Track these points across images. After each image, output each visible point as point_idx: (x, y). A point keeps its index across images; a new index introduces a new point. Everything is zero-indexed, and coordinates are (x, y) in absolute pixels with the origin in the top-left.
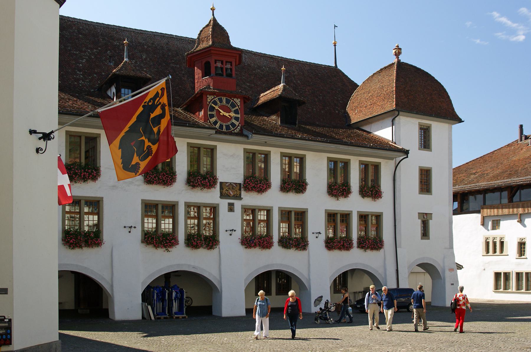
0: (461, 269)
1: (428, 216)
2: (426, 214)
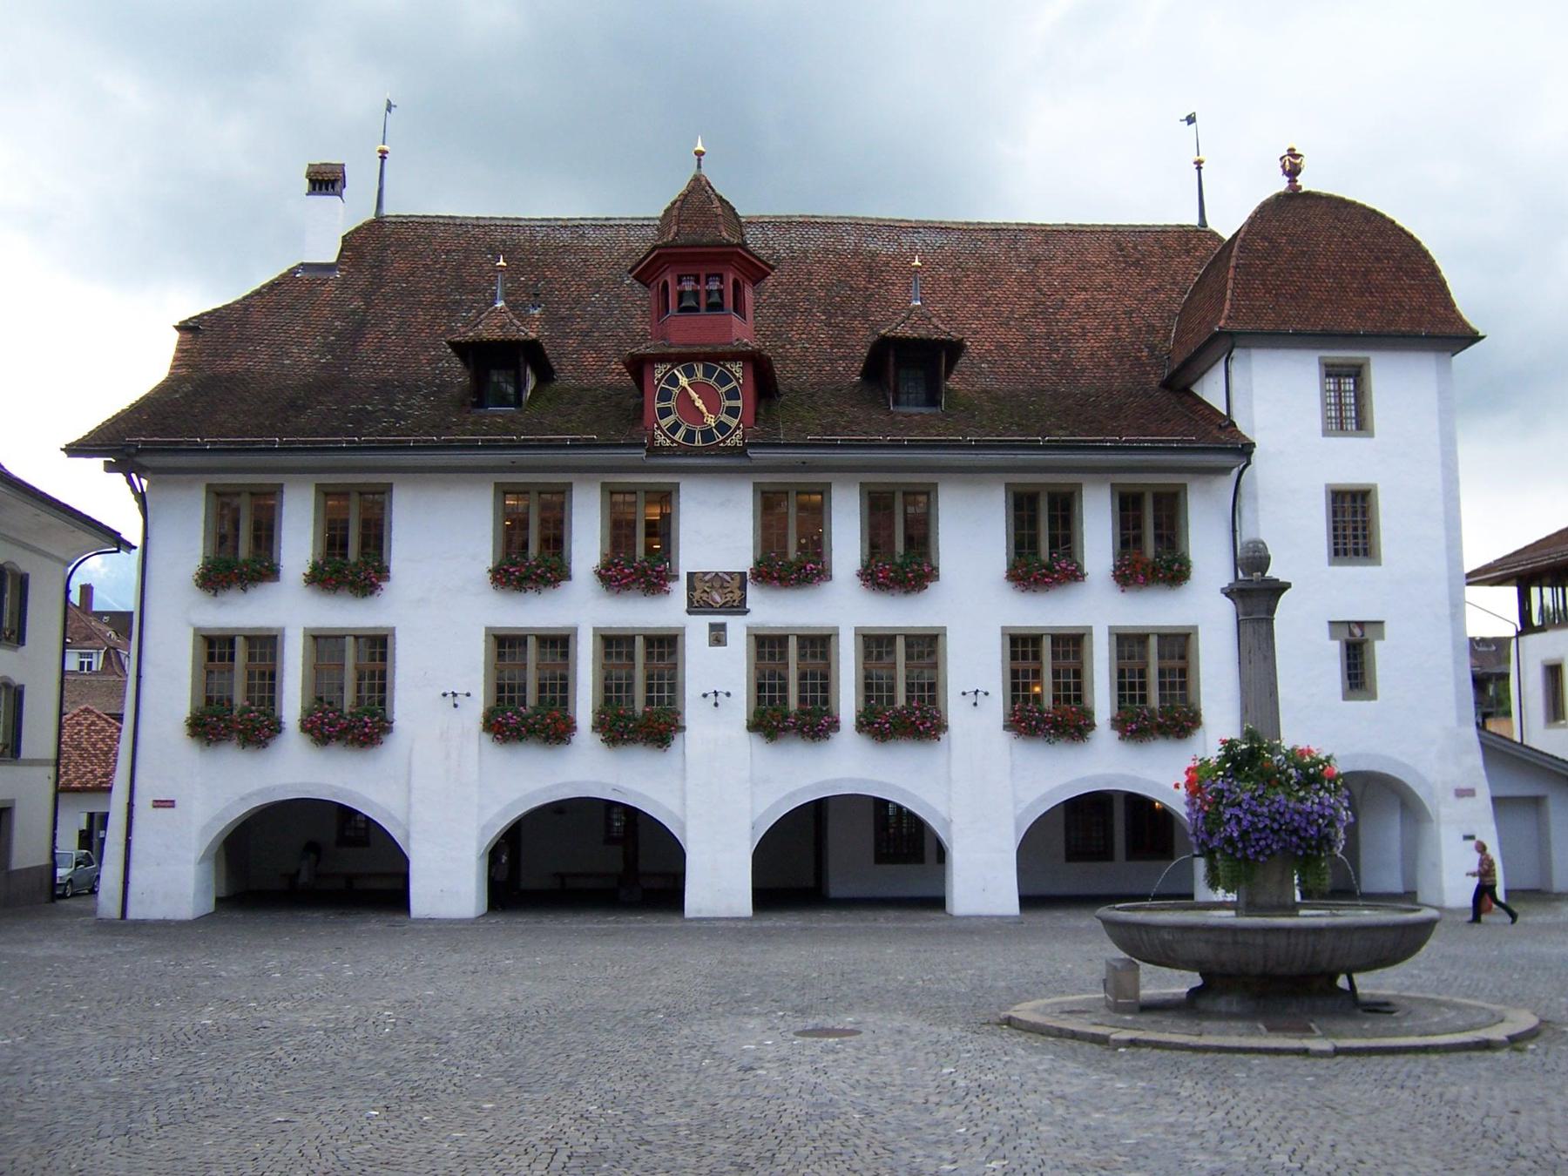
2: (1361, 624)
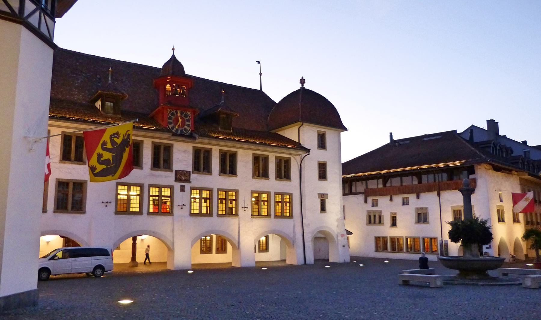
0: (351, 235)
1: (325, 196)
2: (323, 194)
